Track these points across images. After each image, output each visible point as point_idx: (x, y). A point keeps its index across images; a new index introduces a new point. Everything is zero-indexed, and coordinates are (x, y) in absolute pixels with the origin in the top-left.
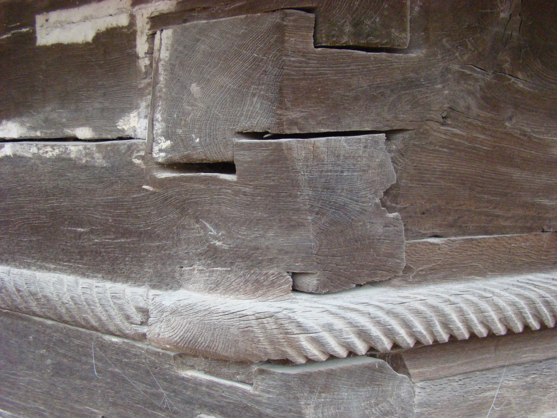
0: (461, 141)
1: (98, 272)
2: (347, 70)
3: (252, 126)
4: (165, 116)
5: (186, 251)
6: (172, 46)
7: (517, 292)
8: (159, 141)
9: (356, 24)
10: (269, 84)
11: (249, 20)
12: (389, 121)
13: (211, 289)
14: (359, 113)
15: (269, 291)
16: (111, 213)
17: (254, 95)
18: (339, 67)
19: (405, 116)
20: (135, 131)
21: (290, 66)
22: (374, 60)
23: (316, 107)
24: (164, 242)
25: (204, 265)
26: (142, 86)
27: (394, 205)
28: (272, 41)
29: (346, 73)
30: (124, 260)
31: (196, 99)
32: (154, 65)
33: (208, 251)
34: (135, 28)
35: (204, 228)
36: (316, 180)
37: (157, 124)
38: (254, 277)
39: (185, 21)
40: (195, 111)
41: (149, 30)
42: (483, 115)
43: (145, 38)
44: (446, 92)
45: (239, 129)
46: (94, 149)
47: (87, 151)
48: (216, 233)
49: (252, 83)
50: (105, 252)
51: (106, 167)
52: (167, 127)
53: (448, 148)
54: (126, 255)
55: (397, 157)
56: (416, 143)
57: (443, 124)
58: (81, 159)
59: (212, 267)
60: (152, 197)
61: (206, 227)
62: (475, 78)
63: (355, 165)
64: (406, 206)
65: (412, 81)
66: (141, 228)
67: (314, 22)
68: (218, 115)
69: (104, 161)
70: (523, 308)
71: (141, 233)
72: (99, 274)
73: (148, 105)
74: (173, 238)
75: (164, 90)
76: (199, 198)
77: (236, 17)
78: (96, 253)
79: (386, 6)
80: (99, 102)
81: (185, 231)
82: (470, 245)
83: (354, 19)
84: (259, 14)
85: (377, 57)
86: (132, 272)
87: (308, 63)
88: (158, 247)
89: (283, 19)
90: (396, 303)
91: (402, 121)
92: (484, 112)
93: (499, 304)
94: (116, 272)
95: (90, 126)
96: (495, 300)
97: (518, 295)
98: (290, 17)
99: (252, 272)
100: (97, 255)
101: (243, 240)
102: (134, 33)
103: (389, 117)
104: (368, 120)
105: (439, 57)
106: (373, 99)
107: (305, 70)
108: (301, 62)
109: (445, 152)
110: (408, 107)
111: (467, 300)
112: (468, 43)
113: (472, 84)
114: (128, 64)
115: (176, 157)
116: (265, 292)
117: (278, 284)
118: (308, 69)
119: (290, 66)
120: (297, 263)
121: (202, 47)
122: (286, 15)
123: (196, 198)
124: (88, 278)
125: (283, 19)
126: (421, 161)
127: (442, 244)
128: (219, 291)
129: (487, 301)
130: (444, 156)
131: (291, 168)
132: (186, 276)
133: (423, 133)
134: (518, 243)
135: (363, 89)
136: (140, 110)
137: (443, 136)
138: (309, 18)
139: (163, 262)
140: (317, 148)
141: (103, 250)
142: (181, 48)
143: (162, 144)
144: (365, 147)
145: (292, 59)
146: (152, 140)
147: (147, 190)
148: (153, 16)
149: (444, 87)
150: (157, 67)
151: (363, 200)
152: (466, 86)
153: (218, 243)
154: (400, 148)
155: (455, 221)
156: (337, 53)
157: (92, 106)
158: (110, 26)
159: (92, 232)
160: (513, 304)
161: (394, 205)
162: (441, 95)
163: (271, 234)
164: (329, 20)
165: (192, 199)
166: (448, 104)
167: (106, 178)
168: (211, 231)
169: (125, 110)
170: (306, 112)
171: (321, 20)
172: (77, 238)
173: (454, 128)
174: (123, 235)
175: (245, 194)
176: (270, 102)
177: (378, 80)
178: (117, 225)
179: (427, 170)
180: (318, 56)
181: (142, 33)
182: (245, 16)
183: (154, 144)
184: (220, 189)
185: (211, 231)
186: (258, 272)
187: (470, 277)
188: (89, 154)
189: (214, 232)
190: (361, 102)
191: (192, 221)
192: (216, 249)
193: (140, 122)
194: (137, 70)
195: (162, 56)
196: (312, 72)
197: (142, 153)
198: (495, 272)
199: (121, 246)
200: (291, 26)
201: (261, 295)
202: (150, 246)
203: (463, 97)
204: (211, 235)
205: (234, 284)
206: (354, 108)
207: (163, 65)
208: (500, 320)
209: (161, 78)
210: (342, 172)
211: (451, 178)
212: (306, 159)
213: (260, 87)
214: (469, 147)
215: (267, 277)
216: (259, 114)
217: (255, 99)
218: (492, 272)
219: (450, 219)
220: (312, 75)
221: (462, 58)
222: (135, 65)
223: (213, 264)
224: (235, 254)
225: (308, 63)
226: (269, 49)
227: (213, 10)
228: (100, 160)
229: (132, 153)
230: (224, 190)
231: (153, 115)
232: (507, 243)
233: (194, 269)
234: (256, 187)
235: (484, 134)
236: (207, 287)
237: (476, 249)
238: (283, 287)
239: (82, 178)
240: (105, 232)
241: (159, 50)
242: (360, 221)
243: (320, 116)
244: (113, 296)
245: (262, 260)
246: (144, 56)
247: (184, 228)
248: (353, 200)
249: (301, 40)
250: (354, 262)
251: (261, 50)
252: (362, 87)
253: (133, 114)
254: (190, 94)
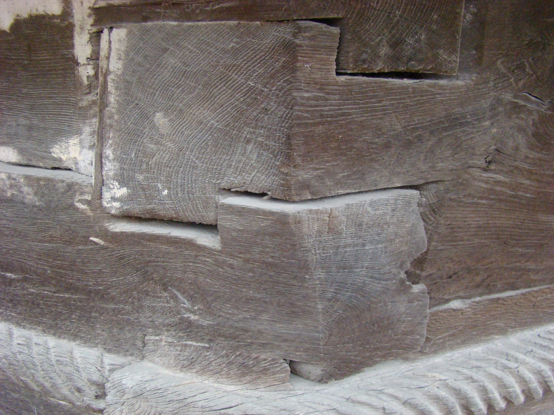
0: (504, 190)
1: (39, 323)
2: (377, 107)
3: (244, 183)
4: (118, 153)
5: (150, 319)
6: (127, 54)
7: (542, 356)
8: (112, 186)
9: (396, 44)
10: (270, 129)
11: (242, 30)
12: (422, 172)
13: (183, 367)
14: (389, 165)
15: (260, 378)
16: (48, 262)
17: (248, 141)
18: (367, 103)
19: (443, 165)
20: (77, 163)
21: (303, 105)
22: (413, 93)
23: (335, 161)
24: (122, 306)
25: (174, 336)
26: (85, 103)
27: (418, 272)
28: (278, 65)
29: (376, 111)
30: (69, 317)
31: (162, 136)
32: (101, 79)
33: (180, 323)
34: (71, 21)
35: (174, 297)
36: (330, 259)
37: (107, 163)
38: (240, 360)
39: (146, 19)
40: (161, 153)
41: (92, 25)
42: (531, 156)
43: (86, 37)
44: (494, 130)
45: (224, 185)
46: (22, 180)
47: (13, 182)
48: (190, 306)
49: (248, 125)
50: (45, 304)
51: (39, 206)
52: (122, 169)
53: (486, 198)
54: (72, 312)
55: (428, 213)
56: (453, 197)
57: (485, 170)
58: (6, 191)
59: (185, 341)
60: (102, 252)
61: (177, 297)
62: (528, 110)
63: (379, 234)
64: (432, 272)
65: (457, 119)
66: (90, 286)
67: (338, 40)
68: (195, 162)
69: (36, 199)
70: (549, 377)
71: (90, 292)
72: (39, 326)
73: (94, 131)
74: (133, 303)
75: (116, 117)
76: (167, 262)
77: (223, 22)
78: (33, 303)
79: (435, 17)
80: (25, 117)
81: (149, 297)
82: (495, 305)
83: (393, 36)
84: (258, 23)
85: (417, 88)
86: (80, 331)
87: (327, 100)
88: (114, 310)
89: (295, 35)
90: (413, 387)
91: (439, 171)
92: (533, 153)
93: (525, 376)
94: (60, 328)
95: (15, 147)
96: (520, 371)
97: (543, 360)
98: (305, 32)
99: (238, 353)
100: (33, 306)
101: (228, 318)
102: (71, 27)
103: (424, 167)
104: (399, 173)
105: (491, 84)
106: (408, 144)
107: (322, 110)
108: (316, 99)
109: (484, 204)
110: (448, 153)
111: (490, 375)
112: (526, 64)
113: (525, 117)
114: (63, 70)
115: (136, 209)
116: (255, 379)
117: (272, 372)
118: (326, 108)
119: (303, 105)
120: (299, 351)
121: (172, 61)
122: (300, 30)
123: (163, 262)
124: (24, 328)
125: (295, 35)
126: (455, 218)
127: (466, 308)
128: (194, 370)
129: (511, 372)
130: (483, 209)
131: (298, 246)
132: (150, 347)
133: (462, 184)
134: (544, 295)
135: (396, 132)
136: (82, 137)
137: (484, 185)
138: (332, 33)
139: (120, 326)
140: (333, 217)
141: (41, 302)
142: (140, 59)
143: (115, 190)
144: (393, 210)
145: (306, 95)
146: (101, 183)
147: (96, 244)
148: (95, 6)
149: (492, 124)
150: (105, 82)
151: (386, 276)
152: (517, 121)
153: (193, 317)
154: (431, 202)
155: (483, 281)
156: (367, 83)
157: (15, 121)
158: (34, 12)
159: (25, 280)
160: (539, 373)
161: (418, 272)
162: (487, 135)
163: (265, 317)
164: (360, 38)
165: (157, 262)
166: (495, 145)
167: (40, 219)
168: (184, 304)
169: (63, 133)
170: (322, 169)
171: (348, 36)
172: (7, 284)
173: (496, 173)
174: (67, 290)
175: (231, 266)
176: (271, 153)
177: (416, 119)
178: (59, 278)
179: (459, 228)
180: (341, 88)
181: (82, 28)
182: (236, 22)
183: (104, 189)
184: (196, 256)
185: (184, 304)
186: (246, 354)
187: (489, 338)
188: (16, 186)
189: (187, 305)
190: (393, 150)
191: (158, 288)
192: (190, 323)
193: (83, 153)
194: (77, 82)
195: (111, 68)
196: (332, 113)
197: (88, 197)
198: (515, 327)
199: (65, 302)
200: (307, 46)
201: (249, 382)
202: (103, 308)
203: (512, 135)
204: (183, 307)
205: (213, 363)
206: (383, 159)
207: (113, 80)
208: (523, 391)
209: (112, 99)
210: (364, 245)
211: (486, 233)
212: (320, 233)
213: (257, 131)
214: (511, 196)
215: (258, 362)
216: (254, 168)
217: (250, 147)
218: (512, 328)
219: (478, 279)
220: (332, 116)
221: (517, 85)
222: (74, 73)
223: (186, 337)
224: (217, 332)
225: (327, 100)
226: (272, 77)
227: (188, 8)
228: (31, 197)
229: (74, 194)
230: (202, 258)
231: (101, 150)
232: (534, 297)
233: (161, 340)
234: (247, 261)
235: (529, 179)
236: (178, 363)
237: (501, 307)
238: (278, 376)
239: (8, 214)
240: (43, 283)
241: (108, 58)
242: (380, 302)
243: (339, 173)
244: (58, 361)
245: (252, 343)
246: (86, 62)
247: (148, 294)
248: (375, 278)
249: (319, 66)
250: (368, 346)
251: (259, 76)
252: (395, 130)
253: (74, 141)
254: (154, 127)
